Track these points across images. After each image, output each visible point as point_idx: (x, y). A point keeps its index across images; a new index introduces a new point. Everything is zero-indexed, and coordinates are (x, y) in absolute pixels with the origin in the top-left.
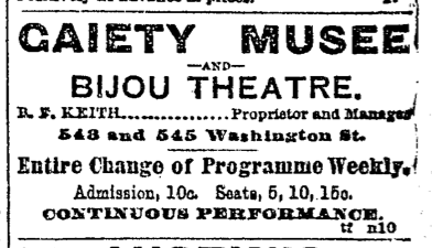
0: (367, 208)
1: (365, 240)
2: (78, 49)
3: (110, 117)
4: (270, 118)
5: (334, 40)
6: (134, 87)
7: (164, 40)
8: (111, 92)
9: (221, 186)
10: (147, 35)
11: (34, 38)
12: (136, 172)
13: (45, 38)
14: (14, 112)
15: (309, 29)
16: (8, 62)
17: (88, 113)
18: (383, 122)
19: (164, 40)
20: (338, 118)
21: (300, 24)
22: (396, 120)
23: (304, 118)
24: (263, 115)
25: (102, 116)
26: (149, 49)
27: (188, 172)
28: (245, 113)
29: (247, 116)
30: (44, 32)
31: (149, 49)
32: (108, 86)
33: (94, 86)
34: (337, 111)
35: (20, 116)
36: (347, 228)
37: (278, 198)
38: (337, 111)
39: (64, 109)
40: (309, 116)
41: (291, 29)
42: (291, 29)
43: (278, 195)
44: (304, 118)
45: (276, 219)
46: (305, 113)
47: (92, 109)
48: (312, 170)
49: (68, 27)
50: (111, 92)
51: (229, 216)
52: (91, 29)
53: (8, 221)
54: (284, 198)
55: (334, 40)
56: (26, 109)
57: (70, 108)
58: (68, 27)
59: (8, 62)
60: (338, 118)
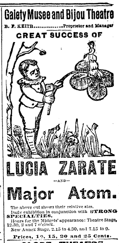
3: (30, 27)
4: (74, 27)
9: (86, 37)
14: (4, 26)
15: (59, 33)
16: (4, 229)
17: (24, 26)
18: (106, 28)
20: (93, 27)
21: (58, 32)
22: (109, 27)
23: (83, 27)
24: (47, 221)
25: (28, 27)
27: (50, 198)
28: (67, 26)
29: (68, 26)
34: (92, 25)
35: (5, 28)
37: (77, 230)
38: (92, 25)
39: (18, 25)
40: (85, 26)
41: (56, 33)
42: (56, 33)
43: (77, 229)
44: (83, 27)
46: (83, 26)
47: (26, 27)
53: (4, 239)
56: (7, 25)
57: (20, 25)
59: (4, 229)
60: (93, 27)
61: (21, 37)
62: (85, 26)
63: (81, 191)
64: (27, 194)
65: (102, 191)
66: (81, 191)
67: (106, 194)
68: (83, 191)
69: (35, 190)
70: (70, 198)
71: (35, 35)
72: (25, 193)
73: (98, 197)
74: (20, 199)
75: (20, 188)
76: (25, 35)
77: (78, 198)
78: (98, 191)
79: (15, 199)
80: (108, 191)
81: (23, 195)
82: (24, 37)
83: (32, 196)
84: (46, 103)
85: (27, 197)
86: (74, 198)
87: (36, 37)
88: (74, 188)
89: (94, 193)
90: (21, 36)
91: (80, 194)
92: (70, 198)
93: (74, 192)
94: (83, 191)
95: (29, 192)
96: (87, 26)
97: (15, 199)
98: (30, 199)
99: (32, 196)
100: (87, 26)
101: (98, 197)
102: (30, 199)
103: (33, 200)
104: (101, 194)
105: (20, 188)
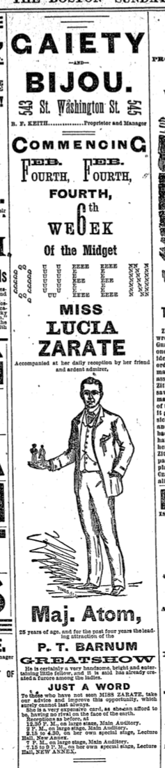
0: (97, 158)
1: (7, 66)
2: (92, 650)
5: (98, 309)
6: (88, 82)
7: (122, 44)
8: (66, 86)
10: (109, 39)
11: (21, 44)
12: (100, 254)
13: (144, 144)
19: (122, 44)
26: (111, 50)
30: (143, 141)
31: (111, 50)
32: (62, 80)
33: (46, 82)
36: (24, 738)
38: (121, 122)
40: (111, 124)
45: (85, 651)
48: (100, 174)
49: (90, 644)
50: (66, 86)
51: (102, 230)
52: (117, 34)
54: (112, 197)
55: (98, 309)
58: (90, 644)
61: (28, 50)
62: (111, 124)
63: (97, 612)
64: (56, 614)
65: (124, 611)
66: (97, 612)
67: (129, 615)
68: (100, 611)
69: (66, 610)
70: (84, 620)
71: (36, 44)
72: (53, 614)
73: (119, 619)
74: (47, 620)
75: (48, 607)
76: (83, 192)
77: (94, 620)
78: (119, 611)
79: (41, 620)
80: (131, 612)
81: (51, 616)
82: (80, 197)
83: (62, 617)
84: (96, 471)
85: (56, 618)
86: (89, 620)
87: (42, 51)
88: (89, 608)
89: (113, 613)
90: (28, 44)
91: (97, 616)
92: (84, 620)
93: (89, 613)
94: (100, 611)
95: (58, 612)
96: (114, 123)
97: (41, 620)
98: (60, 620)
99: (62, 617)
100: (114, 123)
101: (119, 619)
102: (60, 620)
103: (63, 622)
104: (122, 615)
105: (48, 607)
